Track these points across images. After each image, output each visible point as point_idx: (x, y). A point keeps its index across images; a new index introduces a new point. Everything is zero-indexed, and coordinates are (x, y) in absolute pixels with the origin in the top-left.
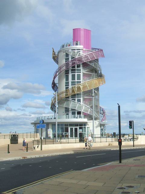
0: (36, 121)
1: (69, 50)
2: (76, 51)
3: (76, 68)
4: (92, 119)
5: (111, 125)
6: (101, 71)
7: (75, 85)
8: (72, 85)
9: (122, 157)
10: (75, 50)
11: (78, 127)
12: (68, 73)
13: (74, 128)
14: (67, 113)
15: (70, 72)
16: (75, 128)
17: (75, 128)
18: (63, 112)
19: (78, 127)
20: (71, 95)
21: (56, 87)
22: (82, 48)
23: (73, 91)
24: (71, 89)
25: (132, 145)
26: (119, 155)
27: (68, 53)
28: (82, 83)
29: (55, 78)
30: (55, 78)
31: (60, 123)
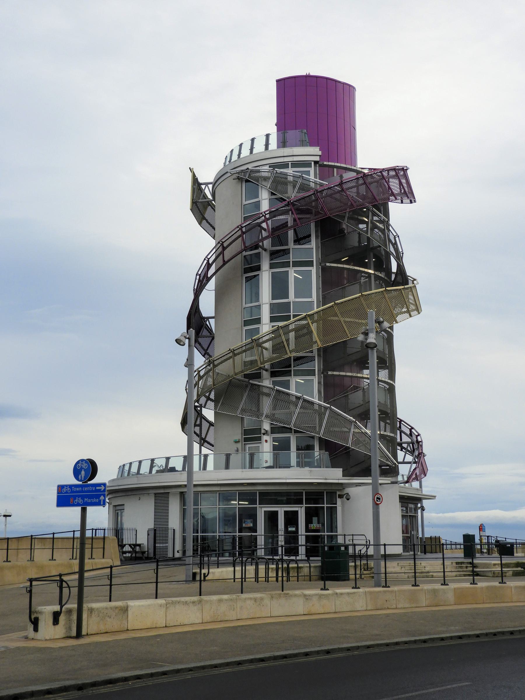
0: (113, 480)
4: (366, 472)
5: (277, 214)
6: (399, 258)
7: (288, 318)
9: (375, 546)
12: (258, 268)
13: (281, 510)
15: (265, 265)
16: (286, 513)
17: (286, 513)
18: (236, 442)
19: (301, 511)
20: (267, 366)
21: (205, 332)
22: (317, 159)
23: (279, 348)
26: (378, 544)
28: (316, 310)
29: (198, 292)
30: (198, 292)
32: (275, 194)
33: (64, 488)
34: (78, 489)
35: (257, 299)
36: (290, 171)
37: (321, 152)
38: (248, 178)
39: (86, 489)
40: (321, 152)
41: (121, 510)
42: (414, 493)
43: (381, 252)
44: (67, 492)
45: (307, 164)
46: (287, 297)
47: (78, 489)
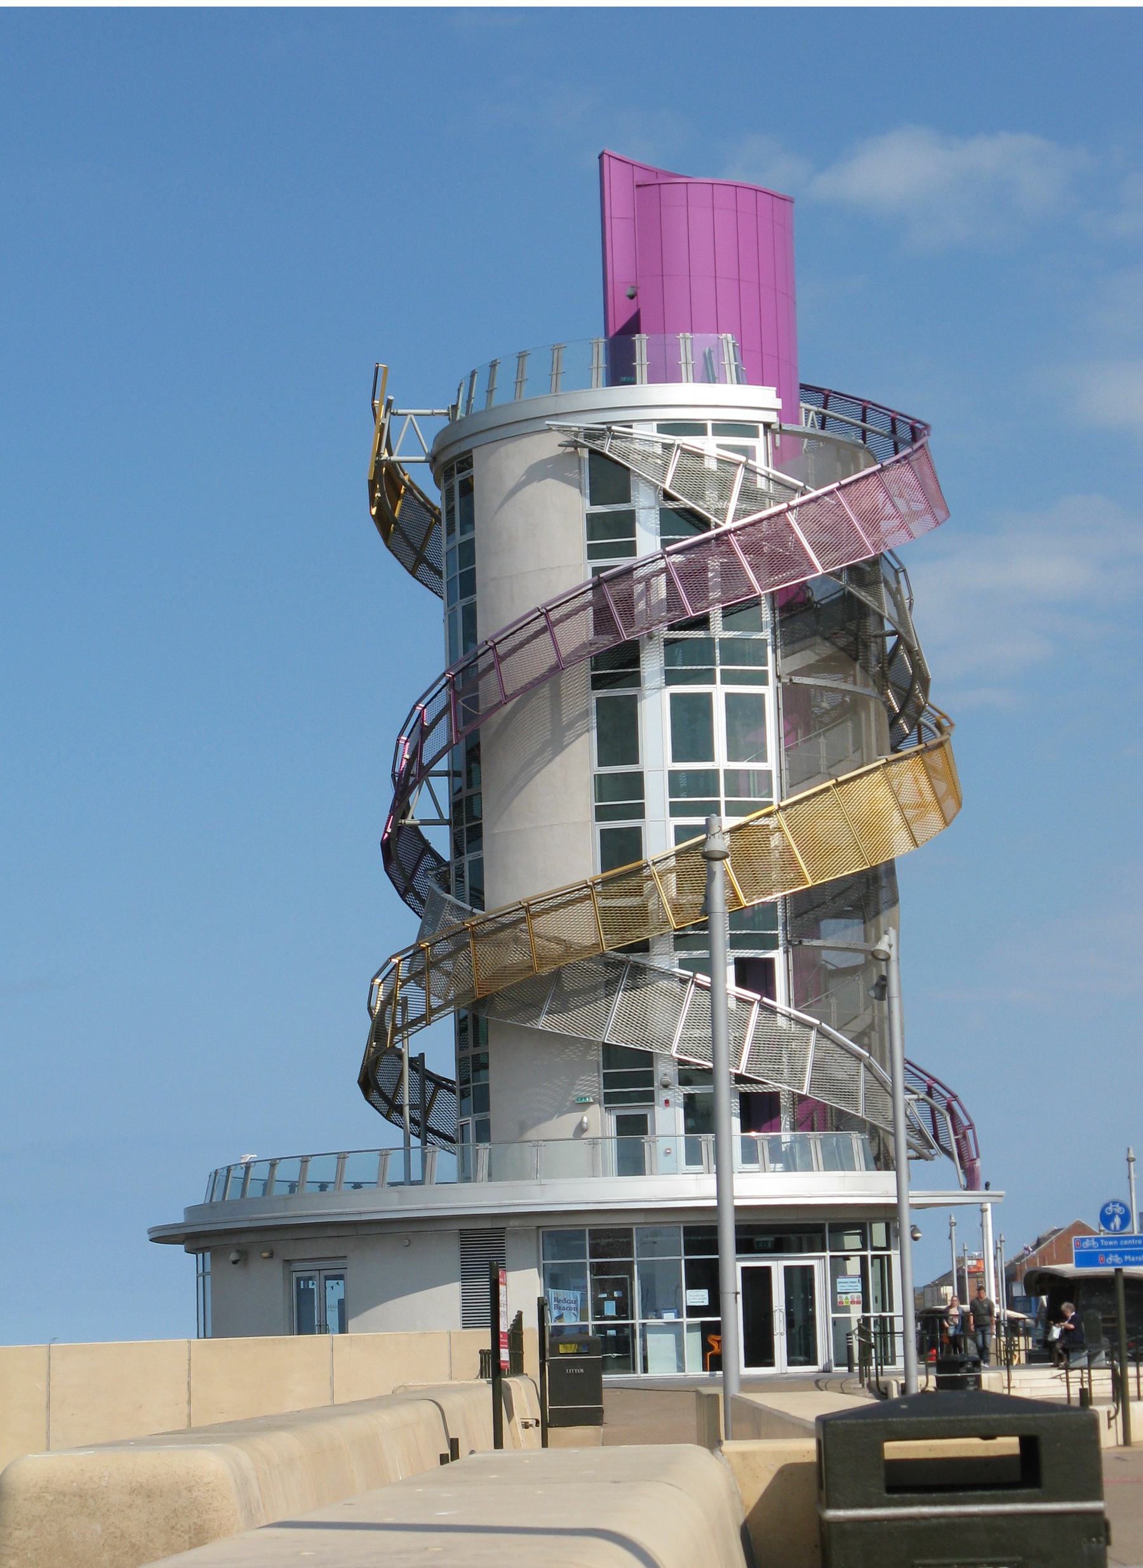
1: (894, 511)
2: (709, 445)
3: (718, 630)
8: (676, 810)
10: (697, 429)
11: (819, 1263)
13: (777, 1267)
14: (632, 1110)
16: (788, 1270)
22: (772, 417)
24: (672, 862)
25: (1135, 1397)
27: (625, 456)
31: (640, 1219)
32: (673, 499)
33: (1085, 1241)
34: (1111, 1243)
35: (632, 756)
36: (709, 445)
37: (780, 400)
38: (609, 451)
39: (1126, 1242)
40: (780, 400)
41: (319, 1270)
42: (495, 1203)
43: (533, 481)
44: (1091, 1247)
45: (745, 429)
46: (709, 756)
47: (1111, 1243)
